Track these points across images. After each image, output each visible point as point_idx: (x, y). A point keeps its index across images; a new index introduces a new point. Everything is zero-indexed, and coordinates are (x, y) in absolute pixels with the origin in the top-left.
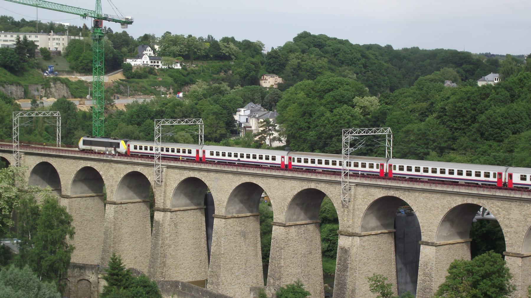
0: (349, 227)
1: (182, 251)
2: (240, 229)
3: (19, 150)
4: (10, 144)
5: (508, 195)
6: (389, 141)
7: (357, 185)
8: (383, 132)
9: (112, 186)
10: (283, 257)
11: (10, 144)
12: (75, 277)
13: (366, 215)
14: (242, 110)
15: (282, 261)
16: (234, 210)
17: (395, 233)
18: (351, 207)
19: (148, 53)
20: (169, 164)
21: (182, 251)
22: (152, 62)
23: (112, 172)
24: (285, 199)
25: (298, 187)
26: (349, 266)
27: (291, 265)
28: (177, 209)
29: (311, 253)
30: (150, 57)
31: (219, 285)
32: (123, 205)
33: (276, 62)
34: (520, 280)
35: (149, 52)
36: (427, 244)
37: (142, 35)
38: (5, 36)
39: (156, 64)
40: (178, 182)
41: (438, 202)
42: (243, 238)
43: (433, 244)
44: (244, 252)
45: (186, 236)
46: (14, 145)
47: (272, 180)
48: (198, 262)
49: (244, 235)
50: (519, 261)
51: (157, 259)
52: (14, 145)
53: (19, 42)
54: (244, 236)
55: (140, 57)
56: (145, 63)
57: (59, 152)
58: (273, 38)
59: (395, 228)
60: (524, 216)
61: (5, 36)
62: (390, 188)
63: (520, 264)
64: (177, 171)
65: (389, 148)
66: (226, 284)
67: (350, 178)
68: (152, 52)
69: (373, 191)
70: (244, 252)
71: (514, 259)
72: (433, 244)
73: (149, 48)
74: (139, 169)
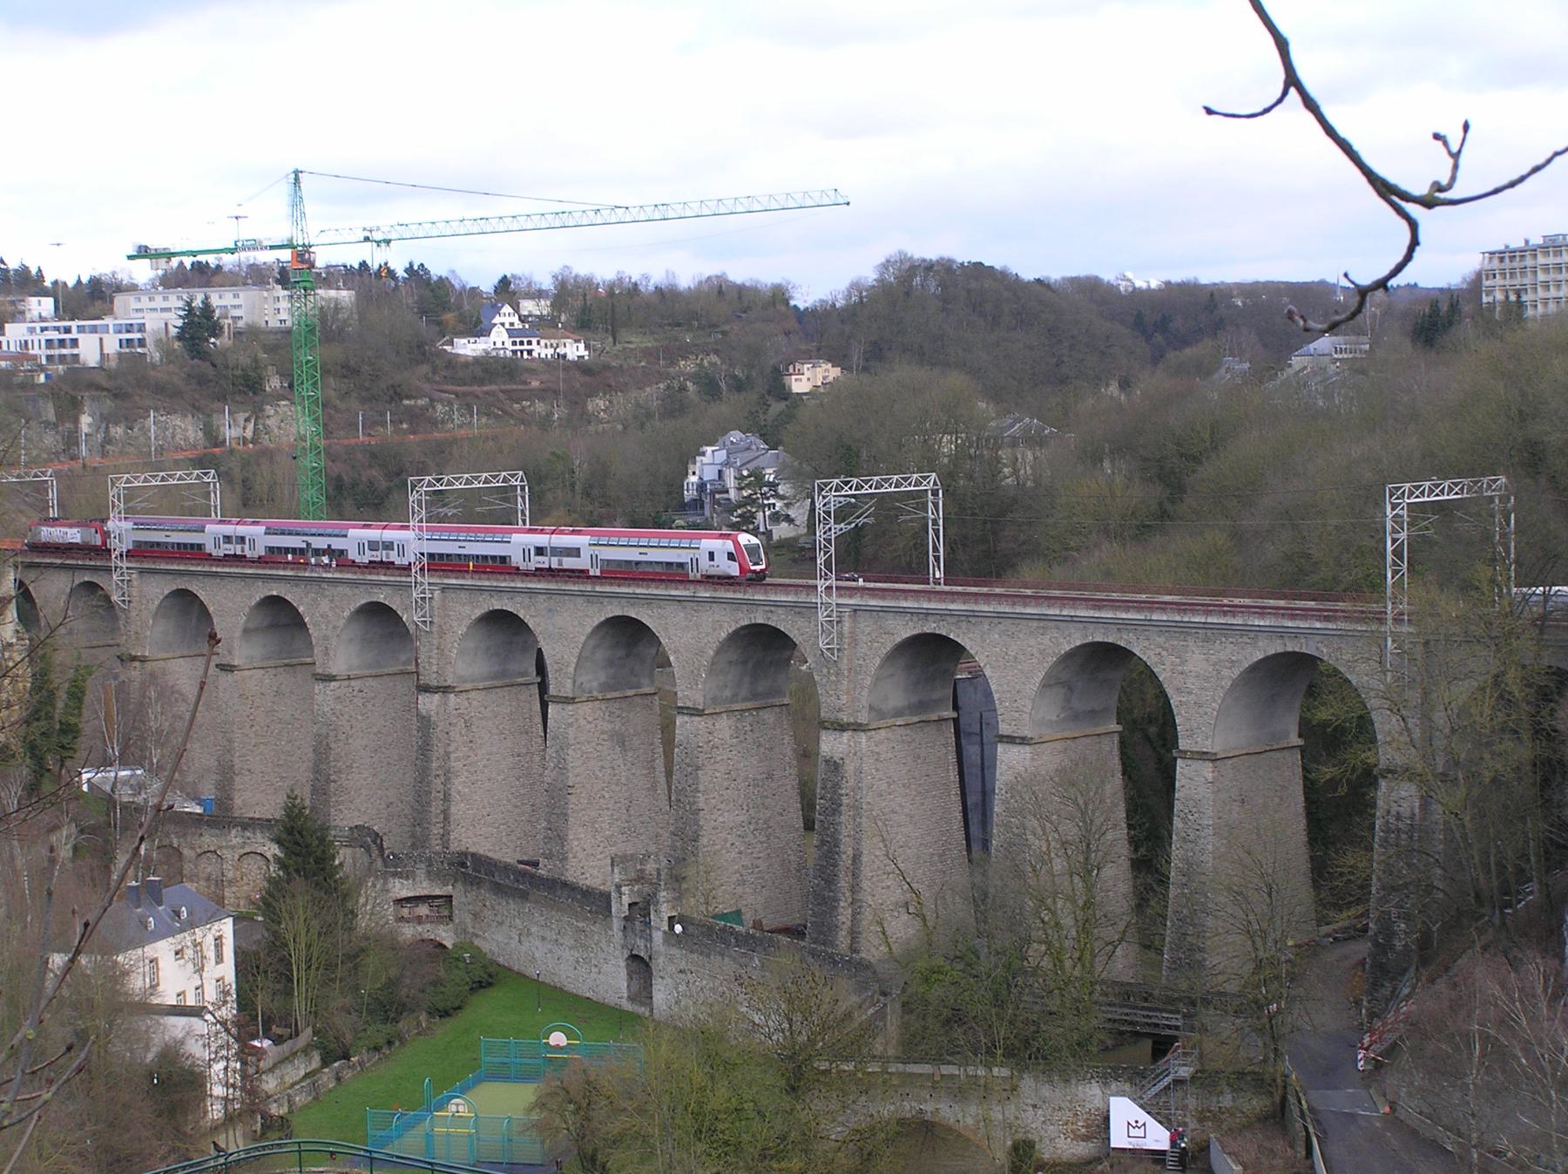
0: (840, 710)
1: (487, 785)
2: (609, 727)
3: (427, 580)
4: (811, 582)
5: (1178, 618)
6: (936, 505)
7: (856, 610)
8: (918, 483)
9: (326, 638)
10: (701, 788)
11: (811, 582)
12: (233, 847)
13: (878, 679)
14: (709, 449)
15: (701, 798)
16: (595, 684)
17: (956, 721)
18: (844, 665)
19: (507, 320)
20: (446, 581)
21: (487, 785)
22: (514, 343)
23: (325, 606)
24: (701, 652)
25: (727, 622)
26: (845, 800)
27: (722, 806)
28: (468, 686)
29: (770, 777)
30: (511, 333)
31: (565, 859)
32: (353, 683)
33: (823, 330)
34: (1210, 812)
35: (506, 316)
36: (1011, 740)
37: (496, 281)
38: (166, 299)
39: (526, 347)
40: (467, 622)
41: (1032, 642)
42: (618, 749)
43: (1023, 741)
44: (623, 780)
45: (494, 749)
46: (821, 584)
47: (671, 608)
48: (528, 808)
49: (621, 740)
50: (1207, 770)
51: (429, 804)
52: (821, 584)
53: (190, 310)
54: (622, 743)
55: (485, 332)
56: (499, 345)
57: (1025, 605)
58: (821, 277)
59: (956, 707)
60: (1215, 664)
61: (166, 299)
62: (499, 591)
63: (1210, 776)
64: (463, 595)
65: (935, 522)
66: (581, 855)
67: (840, 596)
68: (515, 319)
69: (891, 622)
70: (623, 780)
71: (1196, 765)
72: (1023, 741)
73: (507, 309)
74: (381, 597)
